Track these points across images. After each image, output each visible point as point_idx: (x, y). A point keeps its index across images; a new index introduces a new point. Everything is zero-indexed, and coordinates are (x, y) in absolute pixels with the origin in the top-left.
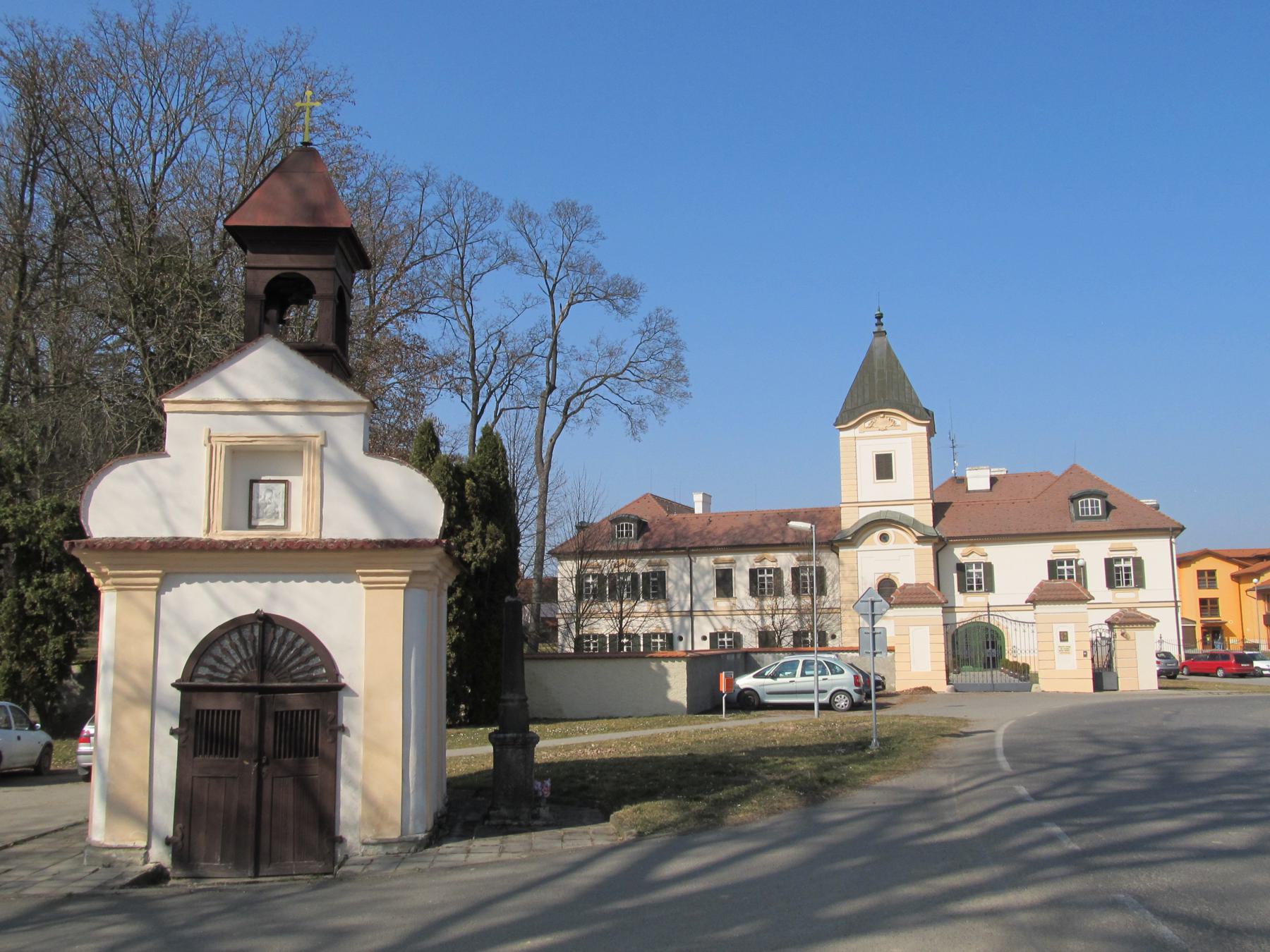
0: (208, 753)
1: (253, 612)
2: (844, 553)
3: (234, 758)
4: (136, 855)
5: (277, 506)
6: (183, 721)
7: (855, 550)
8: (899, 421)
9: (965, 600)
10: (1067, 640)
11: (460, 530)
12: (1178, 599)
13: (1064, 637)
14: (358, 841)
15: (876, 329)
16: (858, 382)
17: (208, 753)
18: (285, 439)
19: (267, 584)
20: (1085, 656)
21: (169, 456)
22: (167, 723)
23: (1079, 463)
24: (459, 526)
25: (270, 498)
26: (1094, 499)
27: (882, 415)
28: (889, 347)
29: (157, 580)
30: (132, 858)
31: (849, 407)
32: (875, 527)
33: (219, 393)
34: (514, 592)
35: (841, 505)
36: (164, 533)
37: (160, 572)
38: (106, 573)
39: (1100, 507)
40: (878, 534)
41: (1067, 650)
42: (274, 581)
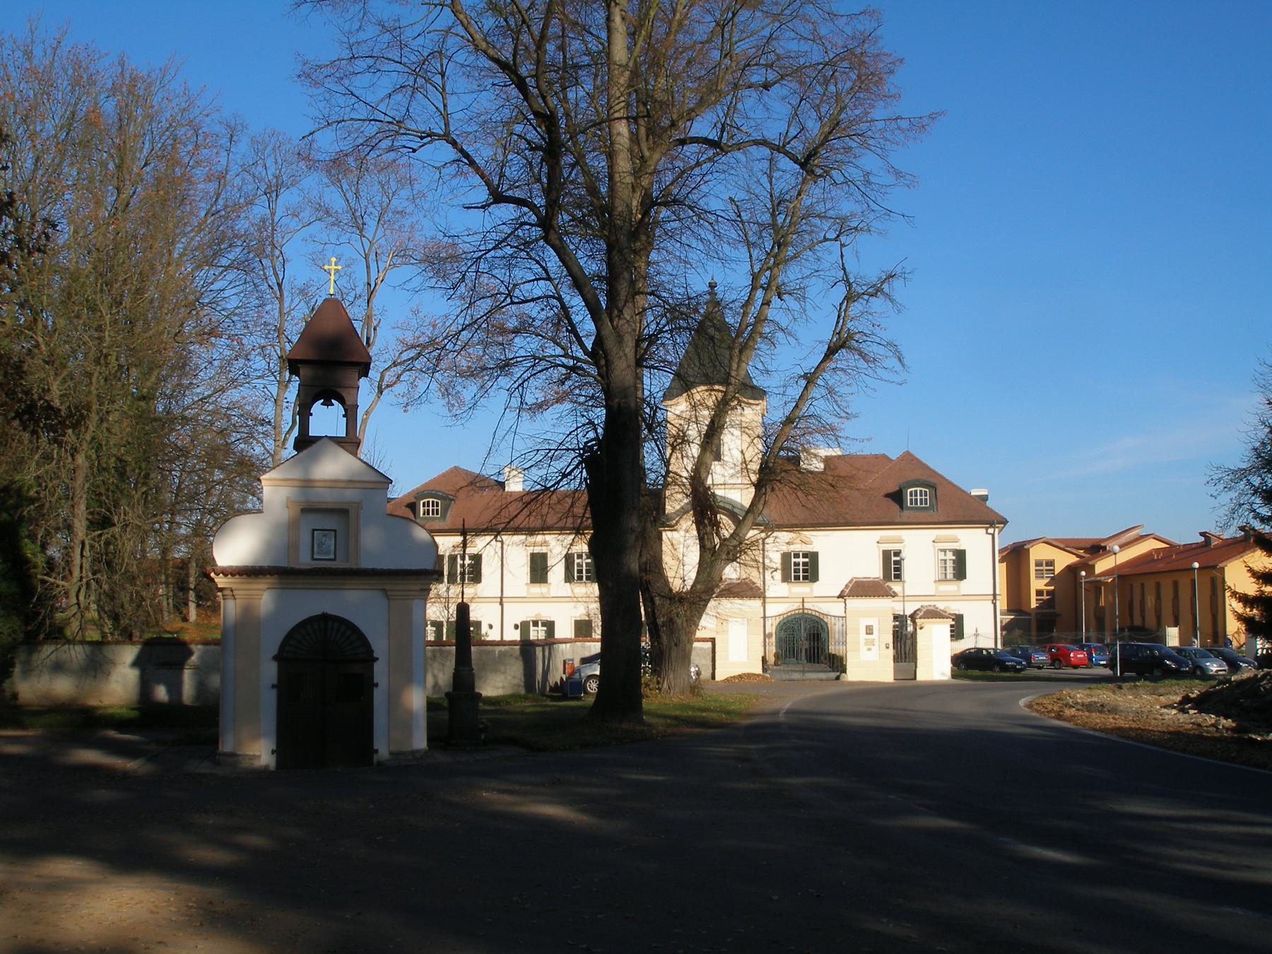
9: (790, 590)
10: (872, 634)
12: (997, 592)
13: (869, 630)
20: (888, 648)
23: (912, 451)
26: (923, 489)
34: (1262, 583)
39: (909, 497)
41: (872, 642)
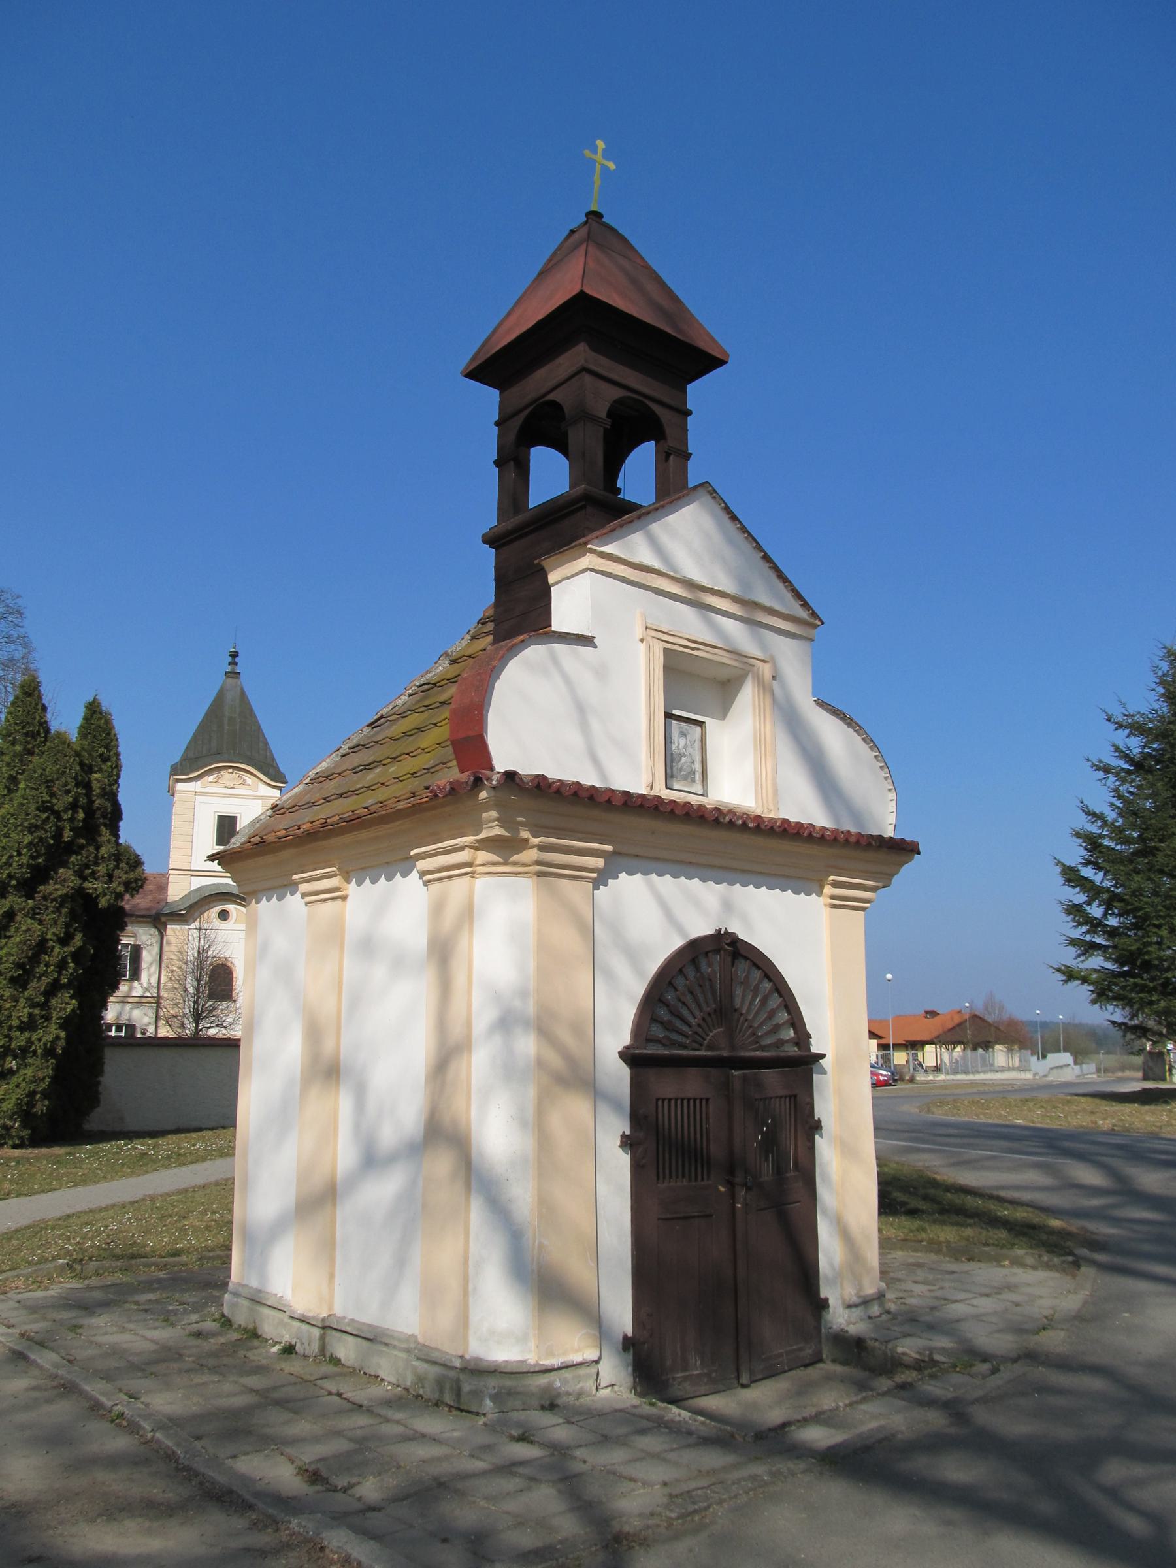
0: (674, 1177)
1: (712, 932)
2: (172, 929)
3: (705, 1183)
4: (579, 1379)
5: (693, 762)
6: (636, 1118)
7: (187, 927)
8: (249, 780)
11: (82, 847)
14: (840, 1302)
15: (229, 669)
16: (203, 727)
17: (674, 1177)
18: (733, 656)
19: (722, 887)
21: (596, 647)
22: (616, 1125)
24: (83, 841)
25: (685, 747)
27: (231, 770)
28: (243, 693)
29: (599, 863)
30: (581, 1385)
31: (191, 755)
32: (215, 901)
33: (646, 556)
35: (170, 872)
36: (590, 779)
37: (610, 848)
38: (527, 840)
40: (215, 911)
42: (732, 884)
